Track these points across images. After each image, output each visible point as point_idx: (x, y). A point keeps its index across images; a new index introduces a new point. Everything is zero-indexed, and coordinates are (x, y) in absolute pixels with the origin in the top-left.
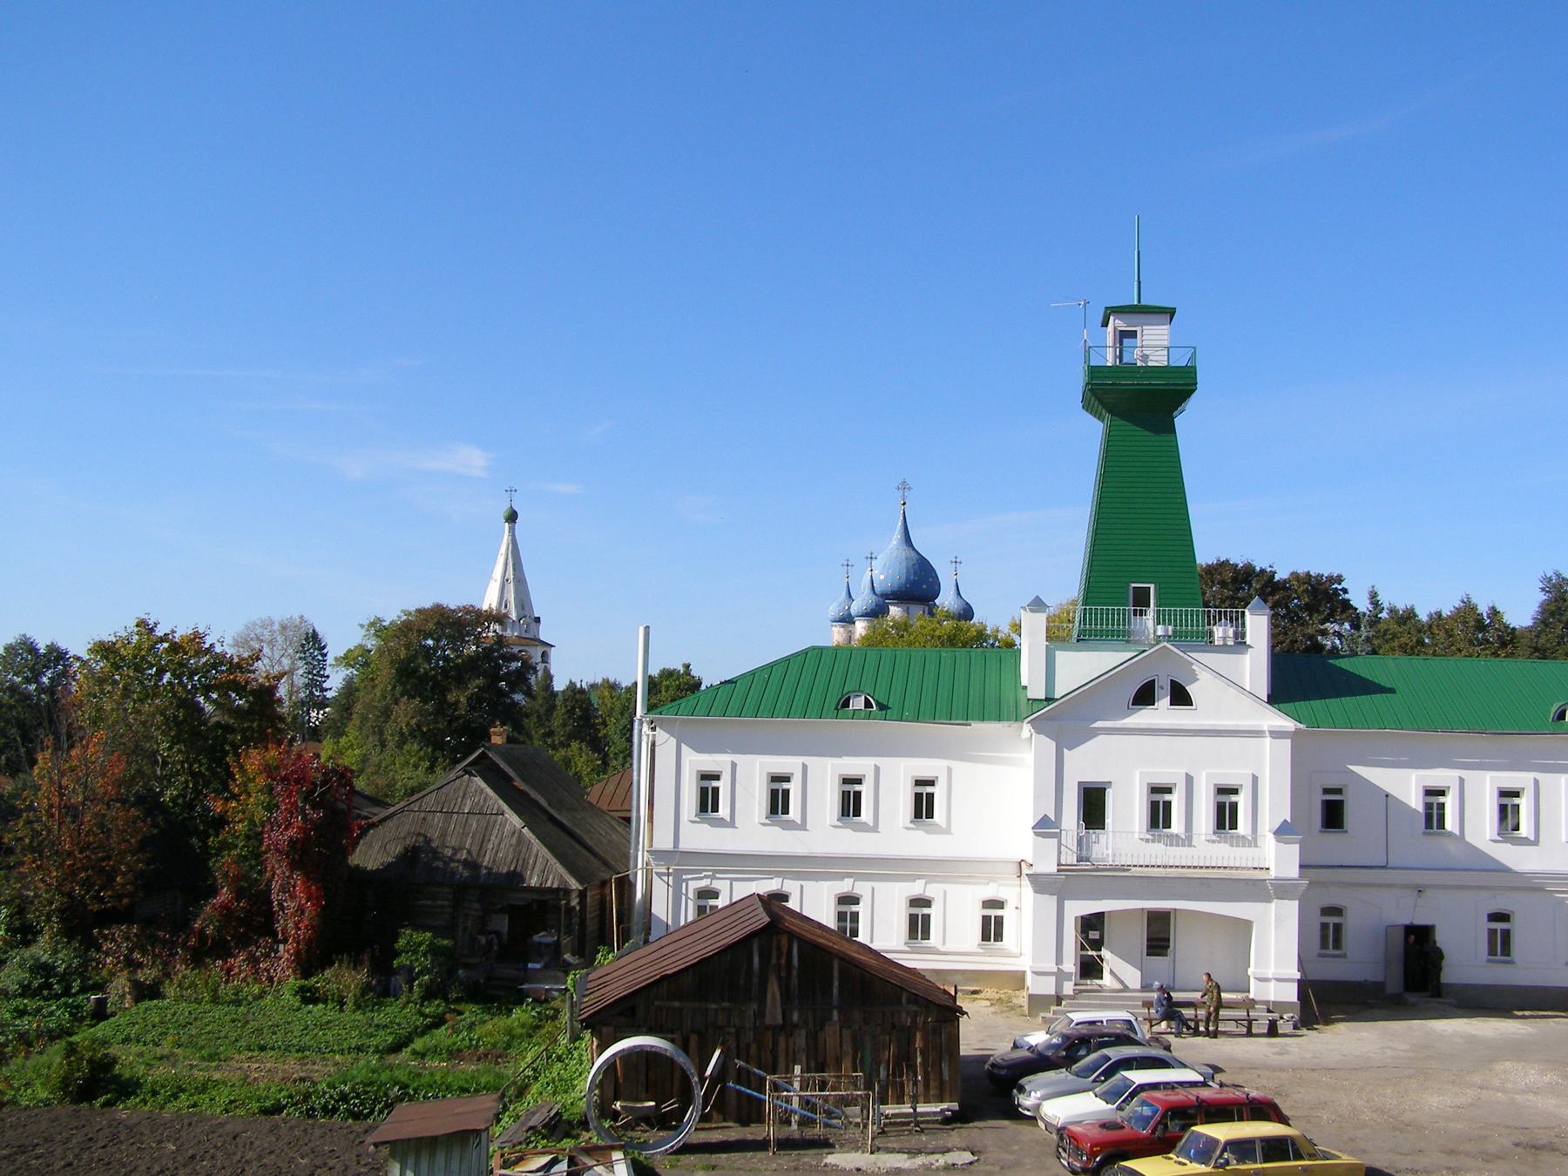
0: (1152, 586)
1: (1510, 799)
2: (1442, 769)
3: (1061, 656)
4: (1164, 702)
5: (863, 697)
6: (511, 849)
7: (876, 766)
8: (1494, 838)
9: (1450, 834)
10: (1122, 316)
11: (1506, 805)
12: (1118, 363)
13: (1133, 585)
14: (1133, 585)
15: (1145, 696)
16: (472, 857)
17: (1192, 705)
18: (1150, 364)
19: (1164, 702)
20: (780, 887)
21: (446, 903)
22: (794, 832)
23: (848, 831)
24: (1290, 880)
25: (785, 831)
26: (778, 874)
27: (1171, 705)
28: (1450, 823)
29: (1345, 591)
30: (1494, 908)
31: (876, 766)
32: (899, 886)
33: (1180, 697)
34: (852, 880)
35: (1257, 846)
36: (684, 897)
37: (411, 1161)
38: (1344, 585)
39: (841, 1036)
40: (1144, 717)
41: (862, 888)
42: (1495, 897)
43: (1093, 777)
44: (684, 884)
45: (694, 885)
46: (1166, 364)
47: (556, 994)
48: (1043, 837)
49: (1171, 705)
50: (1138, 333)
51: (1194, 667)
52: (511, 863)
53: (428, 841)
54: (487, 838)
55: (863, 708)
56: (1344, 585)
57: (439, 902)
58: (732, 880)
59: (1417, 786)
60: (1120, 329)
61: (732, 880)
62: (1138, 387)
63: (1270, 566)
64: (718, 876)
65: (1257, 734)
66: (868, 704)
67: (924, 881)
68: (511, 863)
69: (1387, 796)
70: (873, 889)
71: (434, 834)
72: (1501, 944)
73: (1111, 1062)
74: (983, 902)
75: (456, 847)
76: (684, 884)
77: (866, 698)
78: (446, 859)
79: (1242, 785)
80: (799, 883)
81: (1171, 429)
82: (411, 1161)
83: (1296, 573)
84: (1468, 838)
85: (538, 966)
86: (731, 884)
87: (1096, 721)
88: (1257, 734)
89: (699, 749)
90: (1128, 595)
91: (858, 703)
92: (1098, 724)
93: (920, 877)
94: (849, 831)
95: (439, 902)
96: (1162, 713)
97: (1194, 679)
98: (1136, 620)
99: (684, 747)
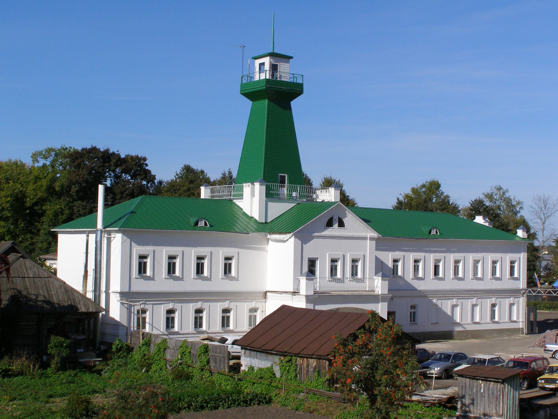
0: (286, 175)
1: (200, 260)
2: (398, 252)
3: (270, 204)
4: (336, 225)
5: (204, 221)
6: (64, 294)
7: (154, 250)
8: (222, 278)
9: (400, 277)
10: (274, 58)
11: (199, 263)
12: (271, 78)
13: (280, 174)
14: (280, 174)
15: (330, 224)
16: (46, 299)
17: (344, 227)
18: (282, 80)
19: (336, 225)
20: (173, 307)
21: (33, 323)
22: (178, 281)
23: (227, 280)
24: (384, 295)
25: (175, 282)
26: (172, 301)
27: (338, 227)
28: (400, 273)
29: (147, 165)
30: (411, 304)
31: (154, 250)
32: (191, 305)
33: (341, 224)
34: (229, 301)
35: (364, 282)
36: (133, 314)
37: (510, 383)
38: (146, 162)
39: (556, 338)
40: (329, 232)
41: (232, 305)
42: (413, 300)
43: (312, 256)
44: (133, 307)
45: (137, 308)
46: (293, 81)
47: (98, 363)
48: (309, 280)
49: (338, 227)
50: (278, 66)
51: (346, 212)
52: (68, 301)
53: (20, 292)
54: (49, 289)
55: (204, 225)
56: (146, 162)
57: (30, 323)
58: (153, 304)
59: (509, 260)
60: (272, 63)
61: (153, 304)
62: (280, 90)
63: (118, 151)
64: (147, 303)
65: (365, 238)
66: (206, 224)
67: (229, 301)
68: (68, 301)
69: (382, 262)
70: (209, 306)
71: (20, 287)
72: (413, 317)
73: (452, 357)
74: (249, 309)
75: (36, 295)
76: (133, 307)
77: (205, 221)
78: (34, 300)
79: (318, 258)
80: (181, 304)
81: (289, 108)
82: (510, 383)
83: (523, 217)
84: (405, 278)
85: (82, 350)
86: (153, 306)
87: (314, 233)
88: (365, 238)
89: (139, 243)
90: (278, 178)
91: (202, 224)
92: (315, 234)
93: (227, 300)
94: (142, 280)
95: (30, 323)
96: (335, 230)
97: (345, 216)
98: (282, 189)
99: (132, 242)
